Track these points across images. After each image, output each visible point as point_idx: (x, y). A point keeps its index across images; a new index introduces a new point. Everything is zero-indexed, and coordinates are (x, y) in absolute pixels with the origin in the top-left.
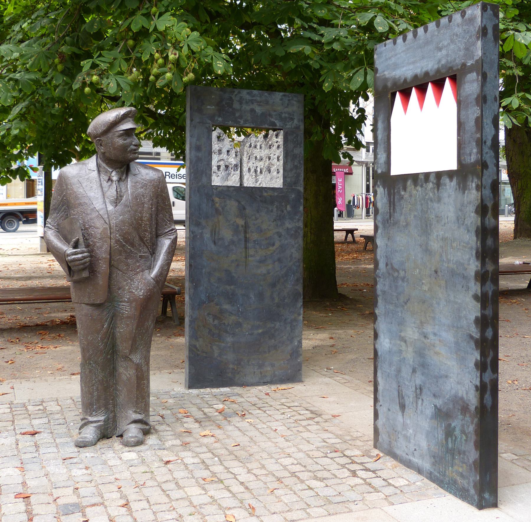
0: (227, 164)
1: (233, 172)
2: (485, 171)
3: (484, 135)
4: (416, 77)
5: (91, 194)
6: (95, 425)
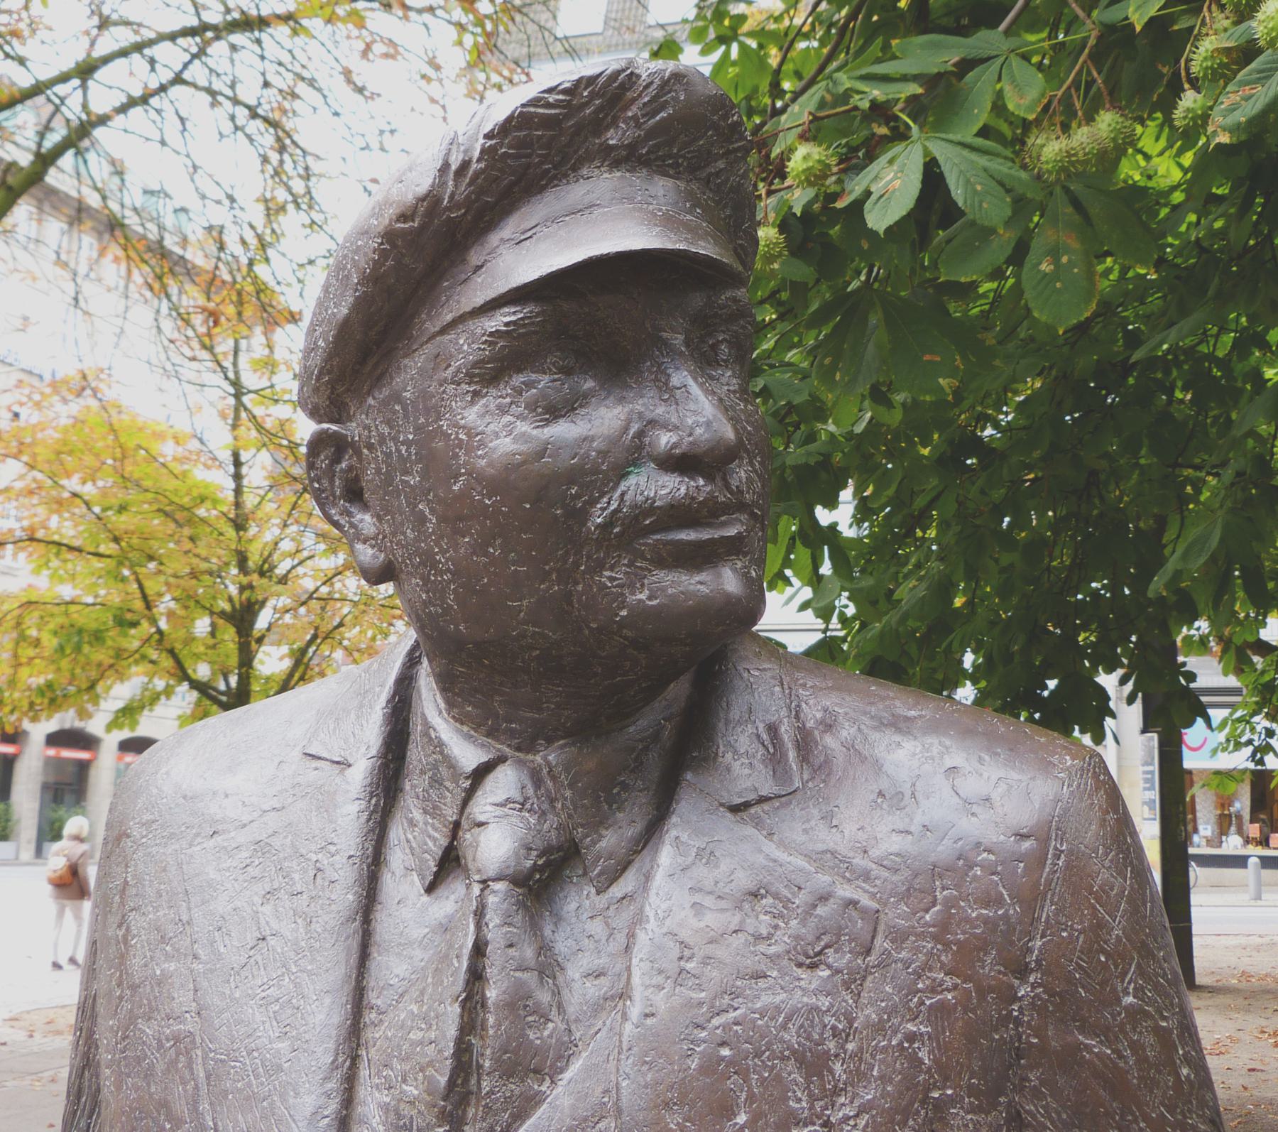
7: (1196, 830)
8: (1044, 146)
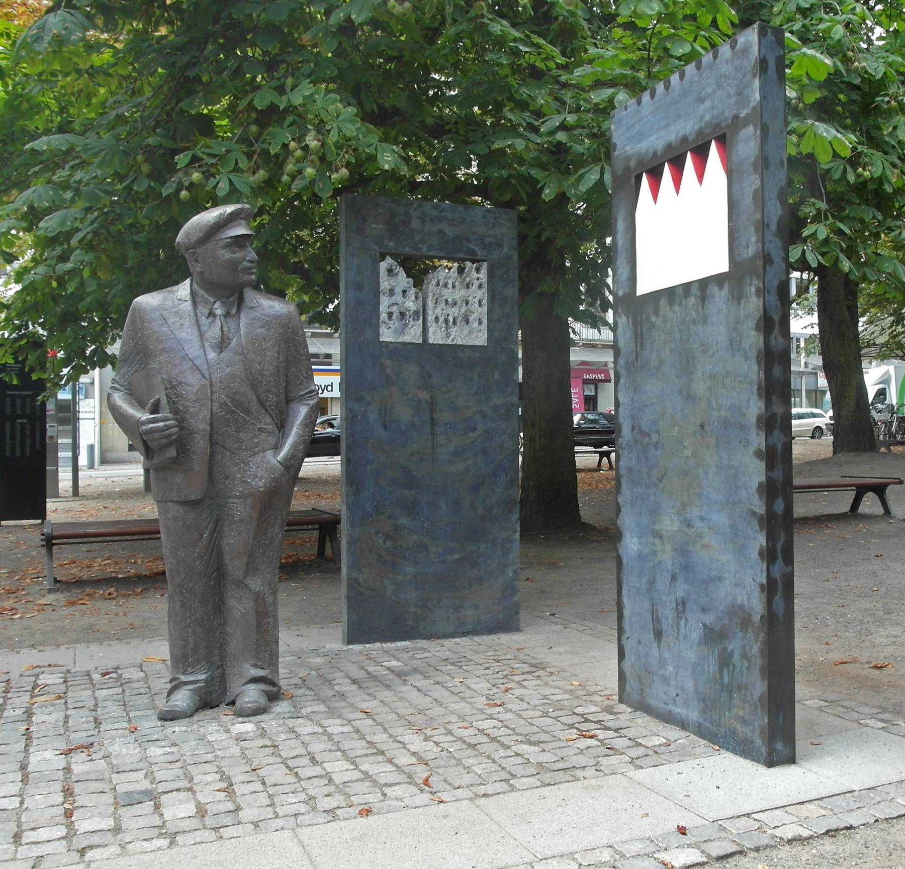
0: (403, 310)
1: (412, 322)
2: (768, 267)
3: (766, 214)
4: (669, 147)
5: (182, 335)
6: (191, 687)
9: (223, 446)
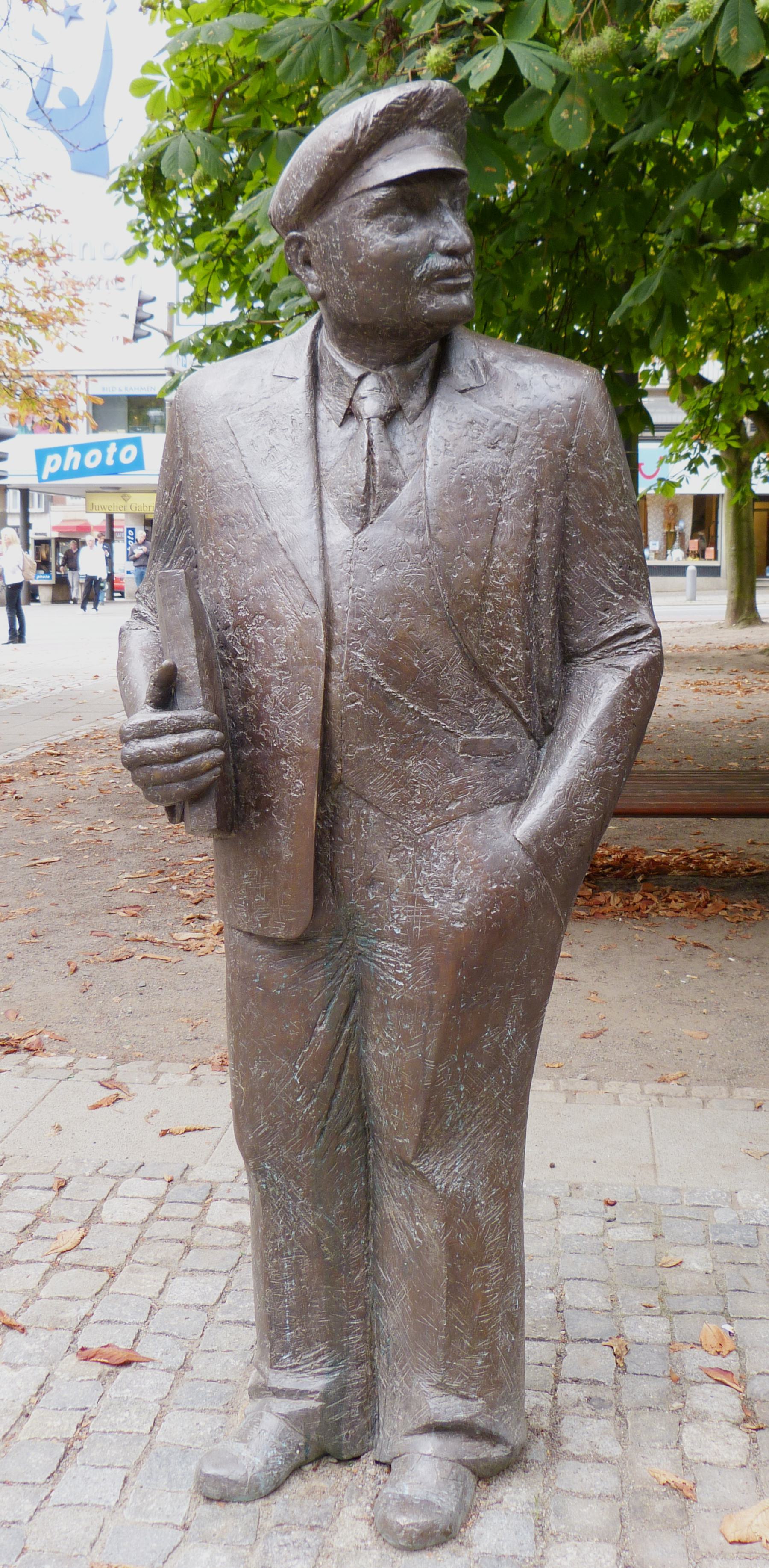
5: (268, 477)
7: (647, 546)
8: (572, 49)
9: (360, 796)
